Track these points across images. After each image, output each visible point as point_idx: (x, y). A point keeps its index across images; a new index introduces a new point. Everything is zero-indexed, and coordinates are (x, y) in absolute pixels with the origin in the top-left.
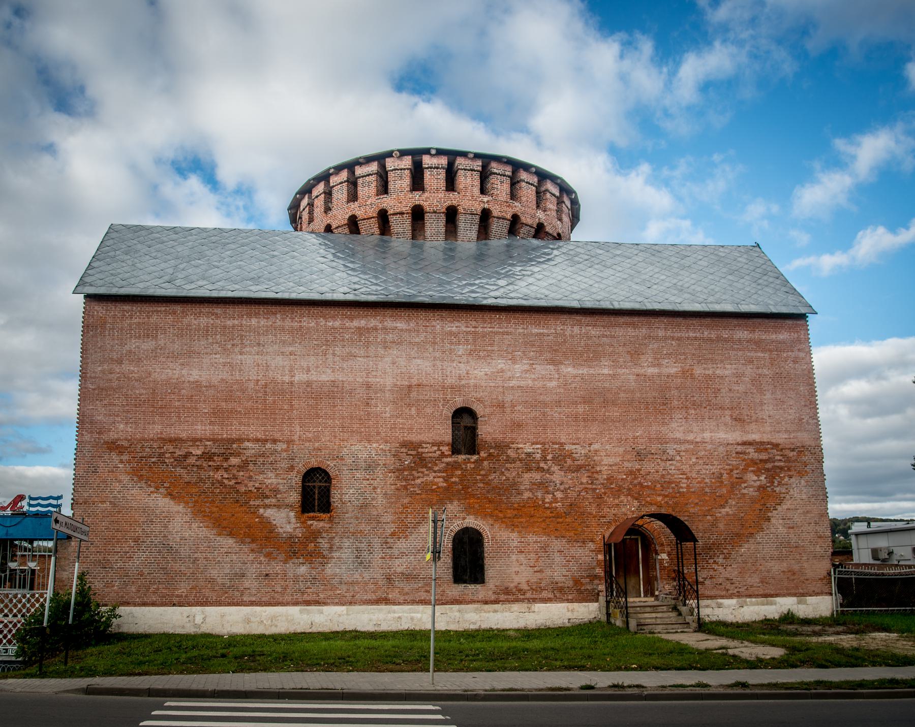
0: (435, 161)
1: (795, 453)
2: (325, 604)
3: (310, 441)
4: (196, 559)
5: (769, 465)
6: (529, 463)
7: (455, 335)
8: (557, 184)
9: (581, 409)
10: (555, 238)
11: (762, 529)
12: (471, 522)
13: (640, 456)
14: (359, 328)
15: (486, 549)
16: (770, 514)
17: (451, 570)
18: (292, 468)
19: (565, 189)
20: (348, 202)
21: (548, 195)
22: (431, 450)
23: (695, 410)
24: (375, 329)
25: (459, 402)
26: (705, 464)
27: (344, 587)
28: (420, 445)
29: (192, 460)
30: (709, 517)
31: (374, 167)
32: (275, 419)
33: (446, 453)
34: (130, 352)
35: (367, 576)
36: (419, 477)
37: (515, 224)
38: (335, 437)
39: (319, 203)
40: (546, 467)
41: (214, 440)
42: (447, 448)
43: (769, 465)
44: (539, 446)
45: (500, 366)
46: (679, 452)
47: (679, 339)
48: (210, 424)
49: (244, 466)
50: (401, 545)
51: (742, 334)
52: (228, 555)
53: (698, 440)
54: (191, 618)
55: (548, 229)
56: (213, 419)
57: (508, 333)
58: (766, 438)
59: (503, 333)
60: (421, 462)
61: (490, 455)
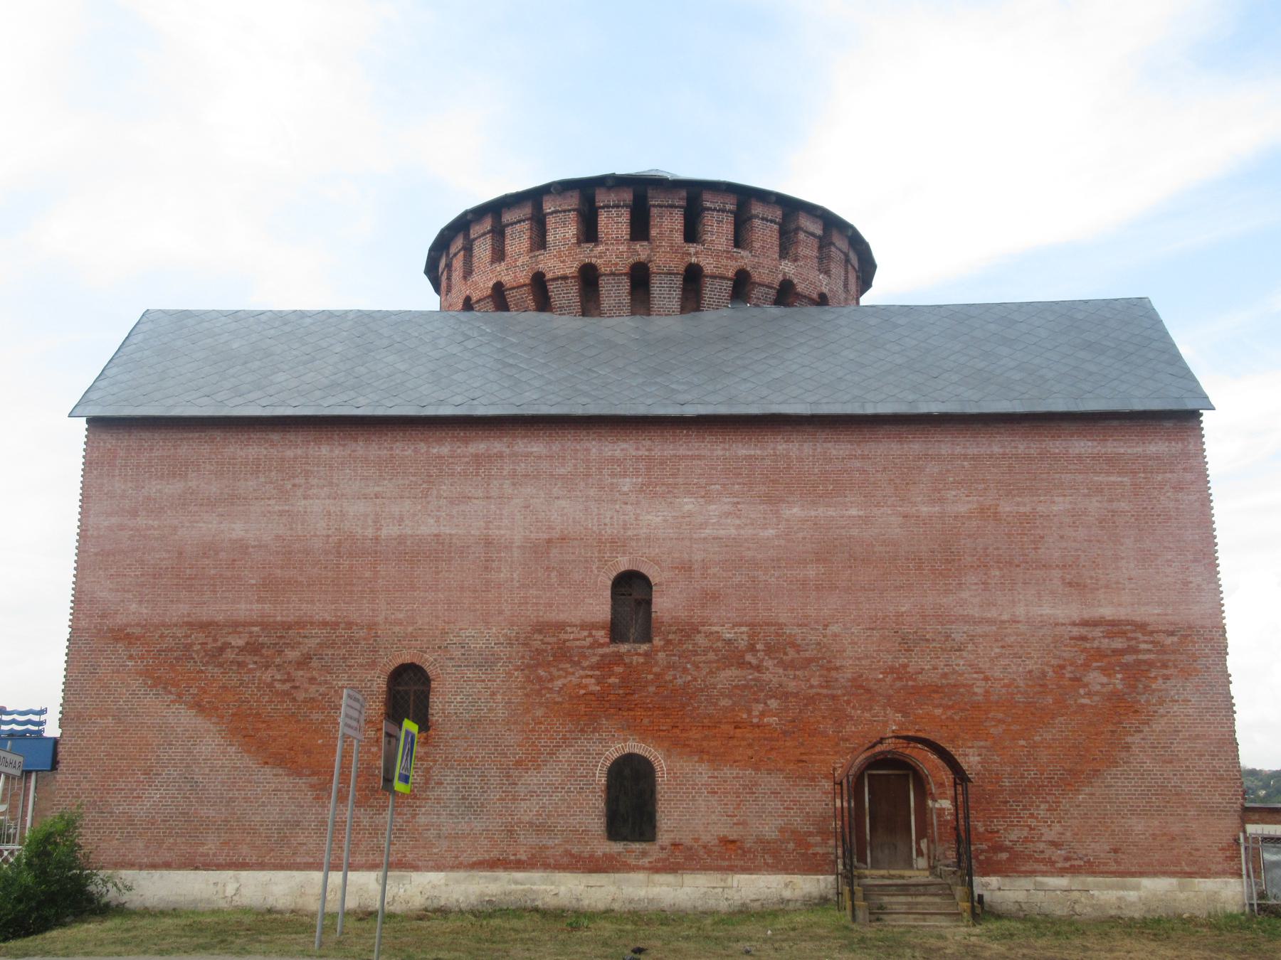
0: (612, 198)
1: (1175, 639)
2: (416, 868)
3: (401, 624)
4: (232, 800)
5: (1129, 658)
6: (734, 657)
7: (619, 462)
8: (817, 216)
9: (811, 572)
10: (814, 303)
11: (1115, 763)
12: (635, 746)
13: (907, 644)
14: (477, 456)
15: (659, 788)
16: (1129, 739)
17: (603, 820)
18: (373, 665)
19: (832, 224)
20: (493, 262)
21: (802, 236)
22: (578, 636)
23: (1001, 569)
24: (500, 456)
25: (624, 564)
26: (1016, 656)
27: (445, 844)
28: (561, 626)
29: (230, 655)
30: (1022, 742)
31: (526, 211)
32: (351, 592)
33: (602, 641)
34: (149, 498)
35: (478, 826)
36: (560, 677)
37: (741, 286)
38: (437, 617)
39: (458, 263)
40: (754, 662)
41: (264, 626)
42: (602, 633)
43: (1129, 658)
44: (744, 629)
45: (687, 508)
46: (972, 638)
47: (975, 458)
48: (258, 601)
49: (304, 662)
50: (532, 779)
51: (1082, 446)
52: (272, 795)
53: (1005, 617)
54: (220, 887)
55: (800, 288)
56: (262, 594)
57: (699, 457)
58: (1123, 613)
59: (693, 458)
60: (562, 654)
61: (668, 642)
